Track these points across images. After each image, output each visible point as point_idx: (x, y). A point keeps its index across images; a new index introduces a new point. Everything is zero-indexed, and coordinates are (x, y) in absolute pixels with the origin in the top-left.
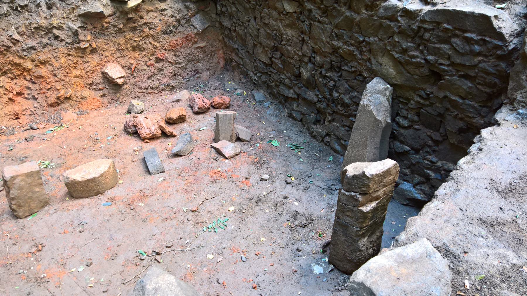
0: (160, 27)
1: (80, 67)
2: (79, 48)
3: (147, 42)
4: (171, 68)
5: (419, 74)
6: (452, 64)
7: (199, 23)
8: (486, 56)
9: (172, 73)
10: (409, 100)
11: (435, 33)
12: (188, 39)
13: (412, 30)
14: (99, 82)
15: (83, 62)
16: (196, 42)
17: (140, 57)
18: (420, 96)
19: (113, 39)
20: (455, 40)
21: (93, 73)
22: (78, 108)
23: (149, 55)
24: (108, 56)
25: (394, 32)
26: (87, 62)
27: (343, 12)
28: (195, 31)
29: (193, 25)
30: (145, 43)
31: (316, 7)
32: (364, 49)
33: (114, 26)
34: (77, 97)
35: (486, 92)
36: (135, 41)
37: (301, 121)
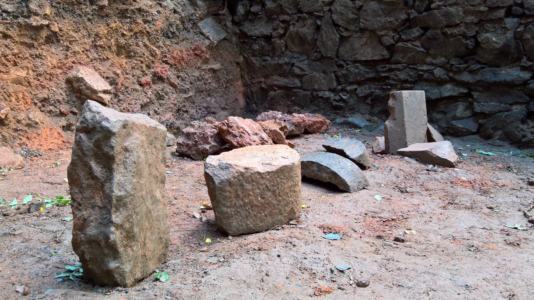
0: (160, 24)
1: (25, 63)
2: (29, 27)
3: (140, 43)
4: (175, 96)
7: (212, 31)
9: (175, 105)
12: (197, 53)
14: (60, 99)
15: (31, 55)
19: (88, 24)
21: (50, 80)
22: (20, 145)
23: (144, 66)
24: (79, 53)
26: (39, 56)
28: (207, 42)
29: (202, 34)
30: (137, 45)
34: (19, 122)
36: (123, 35)
37: (478, 132)
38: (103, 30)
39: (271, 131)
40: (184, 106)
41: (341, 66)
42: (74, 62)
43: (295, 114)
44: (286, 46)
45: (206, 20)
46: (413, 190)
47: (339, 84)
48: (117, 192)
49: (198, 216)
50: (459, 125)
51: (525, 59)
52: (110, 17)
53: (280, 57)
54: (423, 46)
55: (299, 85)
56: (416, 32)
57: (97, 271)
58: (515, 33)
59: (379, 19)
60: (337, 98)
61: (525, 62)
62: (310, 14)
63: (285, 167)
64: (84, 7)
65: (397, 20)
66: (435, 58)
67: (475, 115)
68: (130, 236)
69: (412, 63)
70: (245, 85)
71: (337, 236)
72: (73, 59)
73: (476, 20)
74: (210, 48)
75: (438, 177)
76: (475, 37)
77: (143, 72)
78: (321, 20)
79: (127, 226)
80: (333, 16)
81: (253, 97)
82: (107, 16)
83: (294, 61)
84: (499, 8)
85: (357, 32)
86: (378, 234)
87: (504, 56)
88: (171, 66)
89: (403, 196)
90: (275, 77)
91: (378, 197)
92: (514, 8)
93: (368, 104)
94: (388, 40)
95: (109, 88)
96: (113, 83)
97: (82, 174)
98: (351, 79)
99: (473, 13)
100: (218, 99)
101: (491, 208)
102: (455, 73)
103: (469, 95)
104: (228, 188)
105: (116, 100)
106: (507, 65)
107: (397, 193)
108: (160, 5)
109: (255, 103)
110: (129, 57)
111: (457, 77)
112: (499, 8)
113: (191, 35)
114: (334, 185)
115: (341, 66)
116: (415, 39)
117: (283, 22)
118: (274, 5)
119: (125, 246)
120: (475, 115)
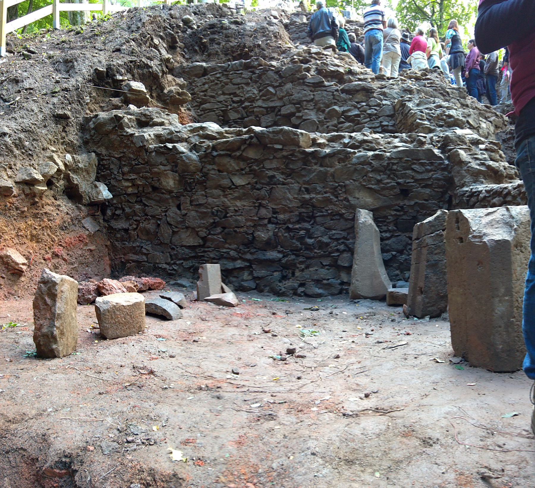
0: (58, 221)
4: (65, 266)
5: (394, 194)
6: (416, 181)
7: (90, 226)
8: (435, 171)
10: (386, 217)
11: (400, 165)
13: (384, 166)
16: (86, 244)
17: (37, 249)
18: (396, 210)
20: (413, 166)
23: (47, 248)
24: (8, 240)
25: (368, 172)
27: (316, 169)
28: (87, 232)
29: (84, 227)
30: (43, 235)
31: (280, 173)
32: (340, 192)
33: (17, 209)
35: (440, 191)
36: (35, 228)
38: (23, 226)
39: (128, 287)
40: (71, 273)
41: (173, 249)
42: (4, 246)
43: (143, 278)
44: (138, 236)
45: (87, 219)
46: (209, 319)
47: (172, 260)
48: (58, 312)
49: (89, 331)
50: (245, 284)
51: (279, 247)
52: (28, 218)
53: (133, 242)
54: (223, 239)
55: (146, 260)
56: (219, 230)
57: (46, 350)
58: (274, 232)
59: (197, 221)
60: (171, 268)
61: (279, 248)
62: (153, 217)
63: (137, 302)
64: (12, 211)
65: (207, 222)
66: (230, 245)
67: (255, 278)
68: (62, 333)
69: (217, 248)
70: (111, 259)
71: (164, 339)
72: (4, 244)
73: (252, 225)
74: (89, 236)
75: (224, 312)
76: (252, 234)
77: (46, 251)
78: (160, 221)
79: (61, 328)
80: (168, 218)
81: (116, 268)
82: (26, 217)
83: (143, 245)
84: (264, 218)
85: (183, 229)
86: (185, 339)
87: (269, 245)
88: (64, 247)
89: (203, 322)
90: (130, 255)
91: (189, 323)
92: (272, 219)
93: (191, 272)
94: (203, 234)
95: (26, 261)
96: (28, 258)
97: (40, 303)
98: (180, 257)
99: (252, 220)
100: (94, 269)
101: (247, 326)
102: (242, 254)
103: (250, 267)
104: (108, 314)
105: (29, 269)
106: (270, 250)
107: (200, 320)
108: (58, 209)
109: (117, 271)
110: (38, 242)
111: (243, 256)
112: (264, 218)
113: (77, 228)
114: (164, 316)
115: (173, 249)
116: (218, 234)
117: (136, 221)
118: (130, 211)
119: (60, 338)
120: (255, 278)
